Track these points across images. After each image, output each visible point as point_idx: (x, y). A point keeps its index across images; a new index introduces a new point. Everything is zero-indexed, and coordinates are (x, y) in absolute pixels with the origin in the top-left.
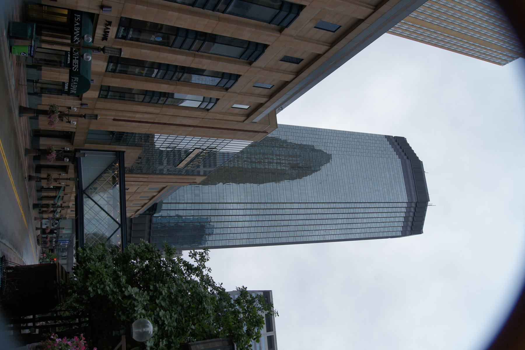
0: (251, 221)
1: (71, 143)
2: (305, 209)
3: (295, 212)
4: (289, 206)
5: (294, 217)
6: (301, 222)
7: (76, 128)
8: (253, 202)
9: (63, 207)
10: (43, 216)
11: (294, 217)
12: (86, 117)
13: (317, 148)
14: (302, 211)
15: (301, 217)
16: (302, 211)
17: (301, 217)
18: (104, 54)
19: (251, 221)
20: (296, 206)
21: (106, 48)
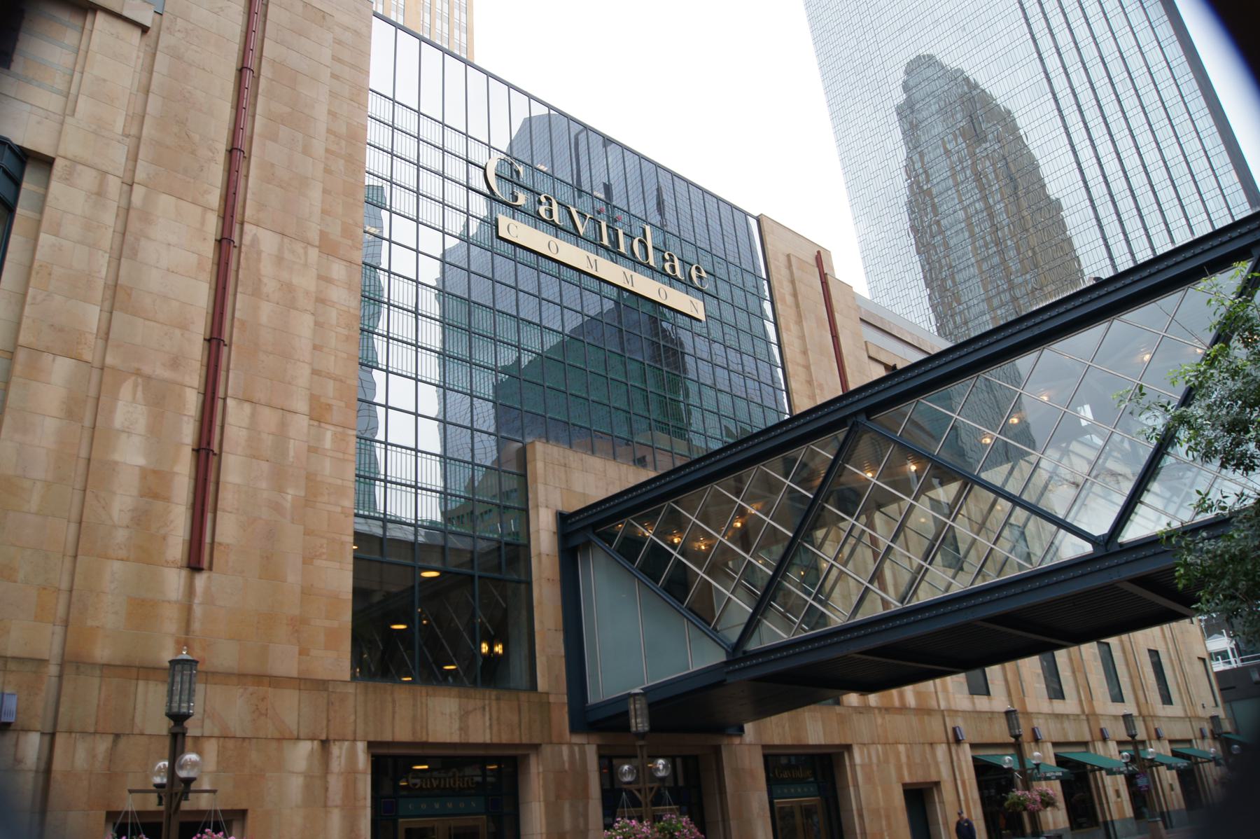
0: (1213, 170)
1: (526, 757)
2: (1142, 54)
3: (1071, 58)
4: (1060, 83)
5: (1090, 52)
6: (1099, 27)
7: (325, 743)
8: (1197, 196)
9: (1017, 737)
10: (1131, 818)
11: (1090, 52)
12: (184, 710)
13: (900, 97)
14: (1063, 38)
15: (1082, 32)
16: (1063, 38)
17: (1082, 32)
18: (192, 714)
19: (1213, 170)
20: (1053, 63)
21: (175, 710)
